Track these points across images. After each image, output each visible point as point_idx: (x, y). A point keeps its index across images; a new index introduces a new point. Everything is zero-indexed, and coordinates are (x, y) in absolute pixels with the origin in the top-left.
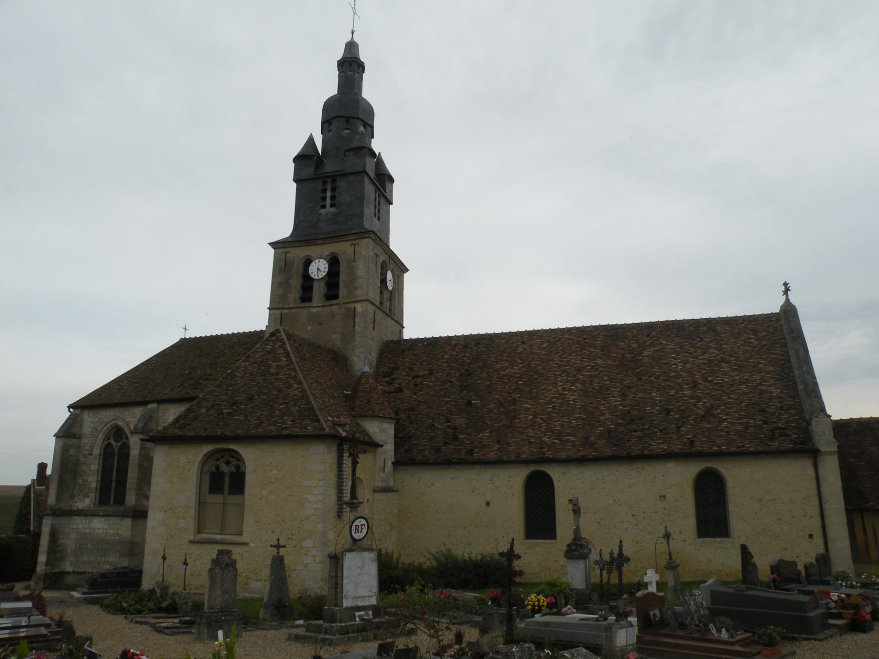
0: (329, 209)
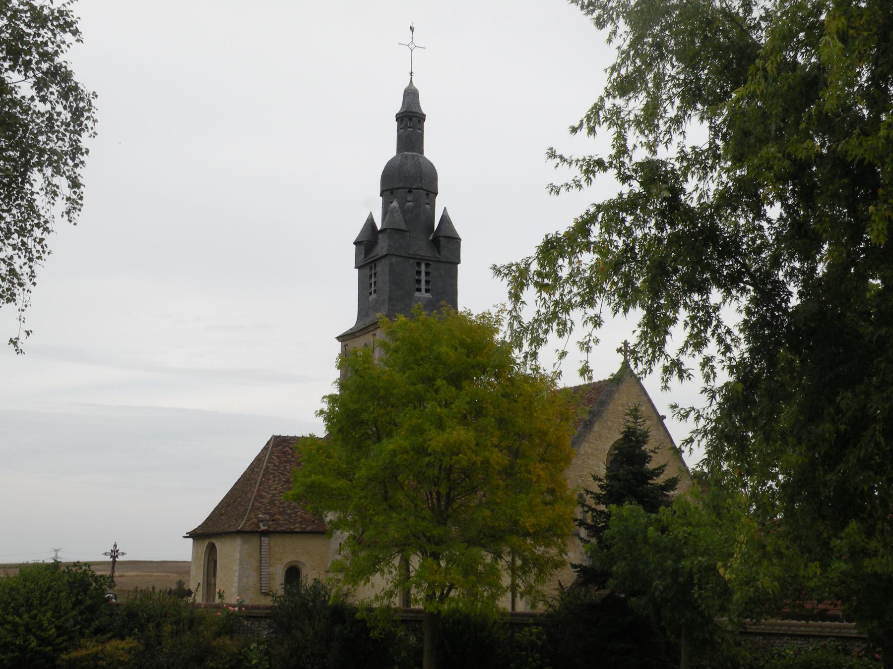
0: (423, 295)
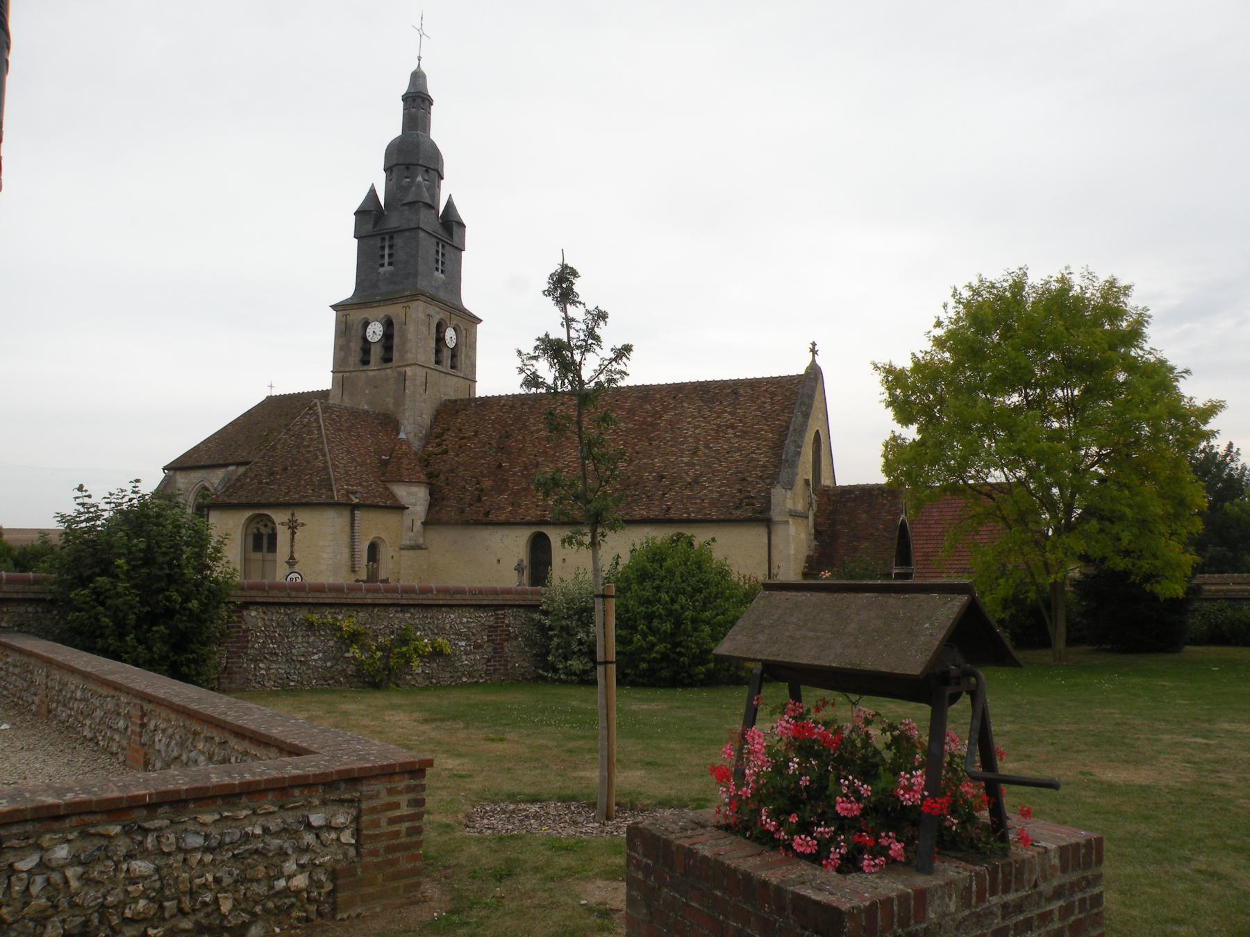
0: (387, 268)
